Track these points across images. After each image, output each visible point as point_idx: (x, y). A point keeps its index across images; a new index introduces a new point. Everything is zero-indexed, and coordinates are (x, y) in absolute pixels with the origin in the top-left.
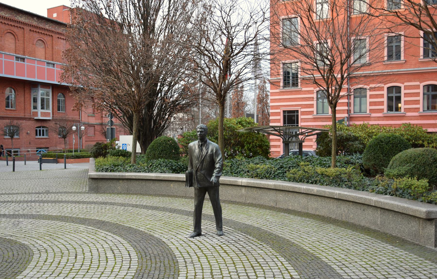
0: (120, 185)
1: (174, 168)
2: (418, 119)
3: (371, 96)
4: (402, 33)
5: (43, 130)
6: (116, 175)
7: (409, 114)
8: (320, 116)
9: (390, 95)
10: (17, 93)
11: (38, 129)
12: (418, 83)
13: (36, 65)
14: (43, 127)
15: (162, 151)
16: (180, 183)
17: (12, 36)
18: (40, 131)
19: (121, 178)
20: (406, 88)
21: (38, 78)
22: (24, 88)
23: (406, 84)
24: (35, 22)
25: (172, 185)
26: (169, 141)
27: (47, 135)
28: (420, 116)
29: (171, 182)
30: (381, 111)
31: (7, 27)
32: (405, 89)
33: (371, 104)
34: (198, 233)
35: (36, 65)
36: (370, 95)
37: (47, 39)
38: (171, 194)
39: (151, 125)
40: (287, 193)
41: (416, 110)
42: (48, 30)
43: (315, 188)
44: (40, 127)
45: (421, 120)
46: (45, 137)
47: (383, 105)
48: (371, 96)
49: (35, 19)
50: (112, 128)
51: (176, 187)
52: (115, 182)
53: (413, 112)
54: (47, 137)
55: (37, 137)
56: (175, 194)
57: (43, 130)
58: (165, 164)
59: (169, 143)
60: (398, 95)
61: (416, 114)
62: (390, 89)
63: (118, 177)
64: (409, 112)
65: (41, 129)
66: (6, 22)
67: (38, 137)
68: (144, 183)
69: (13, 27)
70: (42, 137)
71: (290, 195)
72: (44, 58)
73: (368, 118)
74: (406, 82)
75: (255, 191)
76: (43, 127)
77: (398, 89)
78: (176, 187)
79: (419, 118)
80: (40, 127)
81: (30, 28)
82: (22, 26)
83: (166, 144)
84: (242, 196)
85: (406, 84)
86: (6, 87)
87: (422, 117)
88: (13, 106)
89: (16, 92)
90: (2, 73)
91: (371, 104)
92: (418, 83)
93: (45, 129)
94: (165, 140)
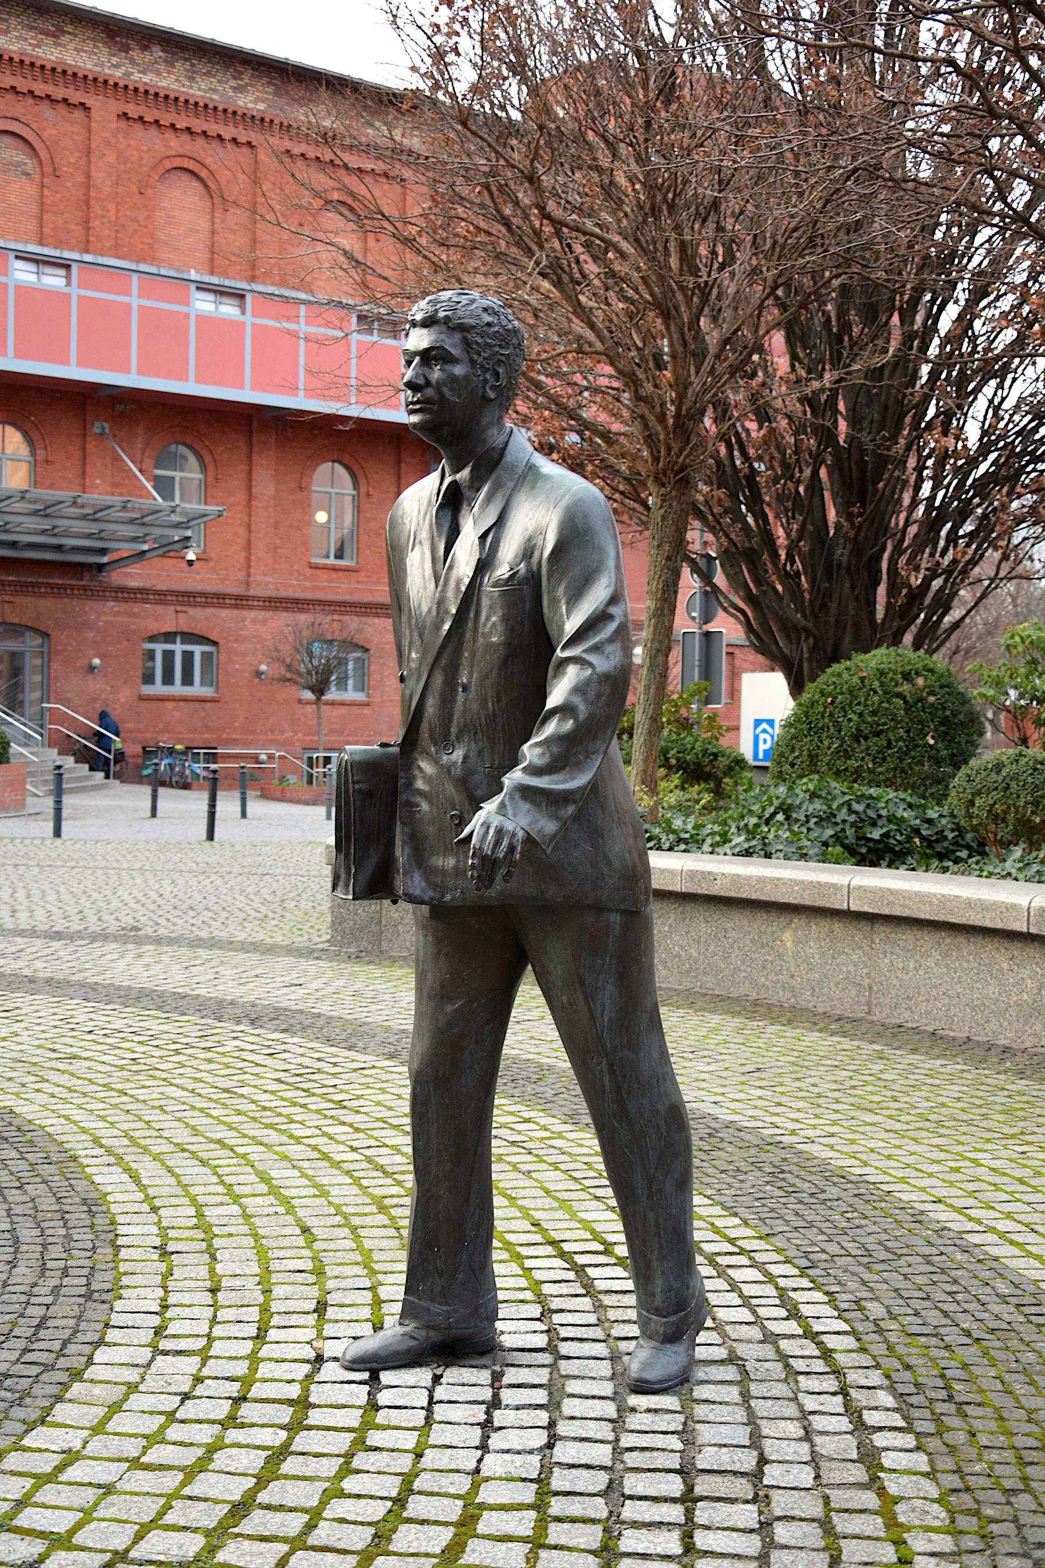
1: (876, 834)
5: (188, 657)
10: (363, 488)
11: (159, 648)
13: (135, 301)
14: (190, 637)
15: (857, 737)
16: (838, 926)
17: (196, 184)
18: (168, 656)
21: (310, 392)
22: (399, 462)
24: (254, 99)
25: (788, 936)
26: (907, 677)
27: (360, 687)
29: (783, 920)
31: (176, 144)
34: (449, 1315)
35: (135, 301)
37: (52, 126)
38: (781, 996)
39: (871, 603)
42: (168, 100)
44: (169, 637)
46: (197, 689)
49: (158, 53)
50: (707, 635)
51: (812, 950)
54: (207, 692)
55: (147, 690)
56: (806, 1000)
57: (188, 657)
58: (818, 806)
59: (905, 688)
65: (178, 648)
66: (198, 125)
67: (158, 688)
69: (201, 141)
70: (177, 689)
72: (203, 256)
76: (190, 637)
80: (169, 637)
81: (117, 106)
82: (76, 96)
83: (889, 694)
86: (317, 458)
88: (347, 552)
89: (362, 482)
90: (128, 371)
93: (198, 650)
94: (882, 673)
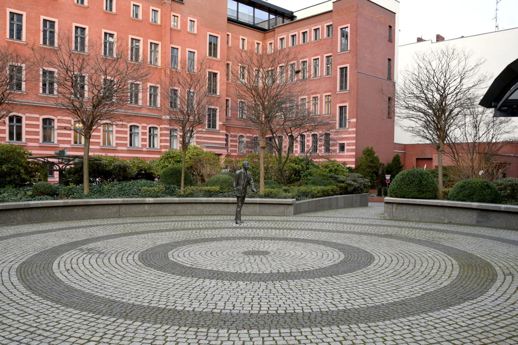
0: (20, 215)
2: (37, 150)
3: (60, 128)
4: (103, 77)
6: (60, 203)
7: (119, 148)
8: (76, 146)
9: (12, 124)
12: (38, 116)
19: (26, 207)
20: (27, 119)
23: (59, 117)
25: (76, 210)
28: (40, 146)
30: (37, 140)
32: (26, 120)
33: (59, 135)
36: (26, 124)
40: (185, 205)
41: (36, 141)
43: (213, 199)
45: (40, 150)
47: (5, 133)
48: (60, 128)
51: (80, 211)
52: (14, 212)
53: (33, 142)
60: (12, 124)
61: (98, 147)
62: (45, 120)
63: (24, 207)
64: (30, 142)
68: (46, 210)
71: (189, 205)
73: (114, 151)
74: (27, 113)
75: (157, 206)
77: (51, 121)
78: (80, 211)
79: (39, 148)
84: (145, 211)
85: (59, 117)
87: (41, 148)
91: (118, 138)
92: (38, 116)
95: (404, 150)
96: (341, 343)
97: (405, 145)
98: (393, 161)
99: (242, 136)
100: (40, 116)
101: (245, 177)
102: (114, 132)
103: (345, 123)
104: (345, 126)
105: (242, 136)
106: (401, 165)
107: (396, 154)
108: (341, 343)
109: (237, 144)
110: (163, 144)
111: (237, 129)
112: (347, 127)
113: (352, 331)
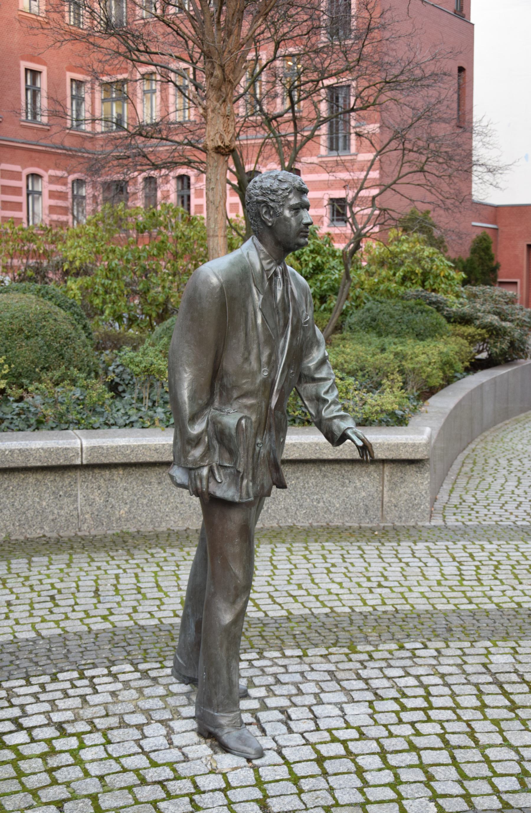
12: (17, 168)
92: (17, 168)
95: (494, 223)
96: (156, 808)
97: (497, 207)
98: (474, 251)
99: (36, 176)
100: (24, 167)
101: (281, 311)
102: (46, 194)
103: (347, 139)
104: (346, 147)
105: (36, 176)
106: (494, 264)
107: (479, 232)
108: (156, 808)
109: (22, 199)
110: (55, 217)
111: (19, 152)
112: (353, 149)
113: (496, 722)
